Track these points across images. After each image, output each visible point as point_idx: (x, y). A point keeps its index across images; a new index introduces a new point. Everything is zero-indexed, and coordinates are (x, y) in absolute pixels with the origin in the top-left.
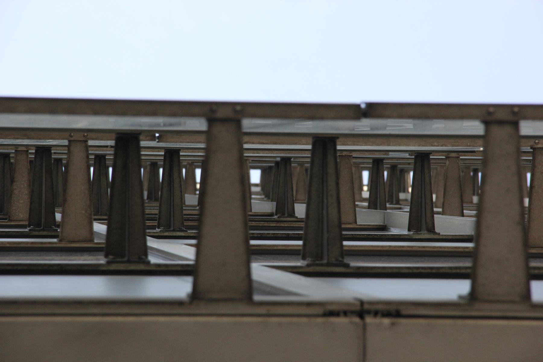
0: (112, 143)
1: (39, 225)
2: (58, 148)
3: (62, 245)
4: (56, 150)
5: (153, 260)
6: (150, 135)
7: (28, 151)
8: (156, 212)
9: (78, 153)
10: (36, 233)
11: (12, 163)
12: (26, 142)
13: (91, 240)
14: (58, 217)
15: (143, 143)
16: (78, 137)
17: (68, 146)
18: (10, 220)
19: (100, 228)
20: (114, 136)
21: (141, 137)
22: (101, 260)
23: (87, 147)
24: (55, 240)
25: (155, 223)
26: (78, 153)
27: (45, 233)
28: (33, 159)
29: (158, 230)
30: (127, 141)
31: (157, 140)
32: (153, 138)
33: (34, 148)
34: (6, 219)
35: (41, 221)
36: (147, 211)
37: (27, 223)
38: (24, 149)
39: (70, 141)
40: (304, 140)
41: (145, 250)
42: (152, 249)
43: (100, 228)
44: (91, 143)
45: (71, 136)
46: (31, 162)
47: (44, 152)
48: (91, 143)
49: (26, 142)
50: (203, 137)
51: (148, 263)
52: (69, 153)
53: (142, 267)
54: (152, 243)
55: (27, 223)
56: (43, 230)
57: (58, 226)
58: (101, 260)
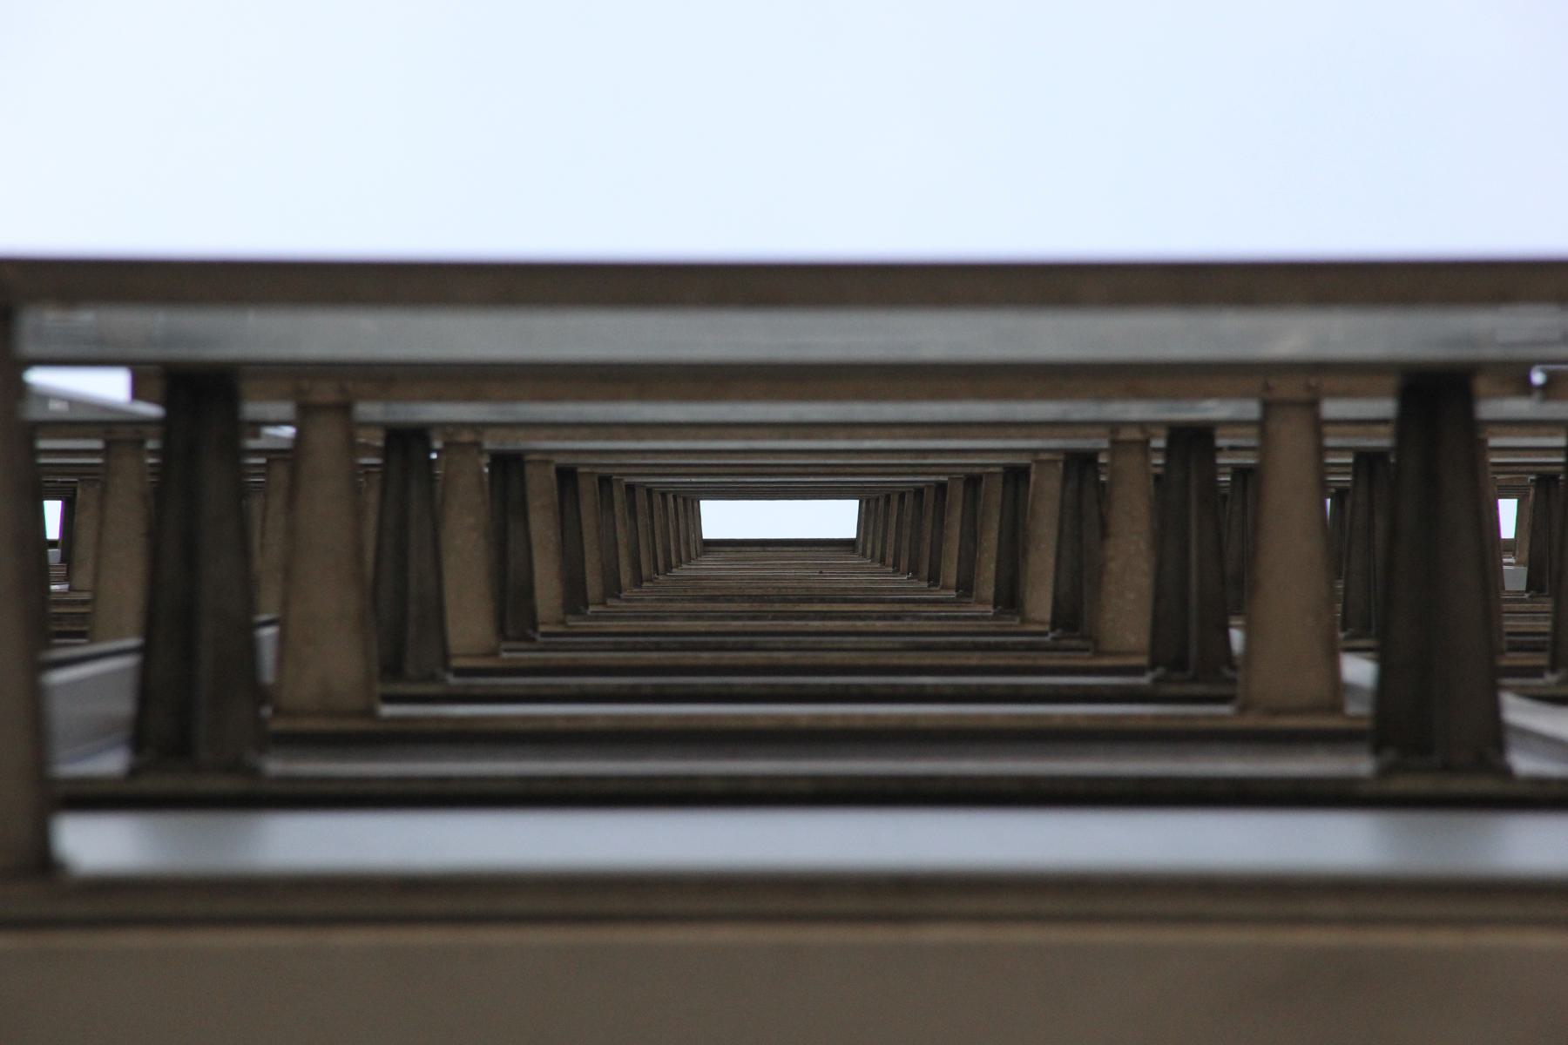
0: (1386, 407)
1: (1179, 664)
2: (1239, 431)
3: (1251, 721)
4: (1234, 436)
5: (1524, 763)
6: (1514, 376)
7: (1147, 442)
8: (1545, 625)
9: (1292, 437)
10: (1173, 690)
11: (1103, 484)
12: (1137, 410)
13: (1336, 708)
14: (1237, 637)
15: (1491, 408)
16: (1288, 389)
17: (1262, 425)
18: (1099, 653)
19: (1359, 670)
20: (1391, 382)
21: (1482, 385)
22: (1360, 765)
23: (1319, 425)
24: (1225, 710)
25: (1542, 660)
26: (1292, 437)
27: (1198, 689)
28: (1382, 440)
29: (1550, 678)
30: (1436, 397)
31: (1537, 395)
32: (1526, 388)
33: (1163, 432)
34: (1086, 650)
35: (1188, 654)
36: (1509, 624)
37: (1143, 660)
38: (1135, 434)
39: (1267, 406)
40: (1250, 453)
41: (1497, 735)
42: (1527, 734)
43: (1359, 670)
44: (1332, 409)
45: (1268, 388)
46: (1158, 478)
47: (1193, 441)
48: (1332, 409)
49: (1137, 410)
50: (1253, 431)
51: (1507, 773)
52: (1265, 446)
53: (1485, 785)
54: (1518, 712)
55: (1143, 660)
56: (1195, 680)
57: (1234, 668)
58: (1360, 765)
